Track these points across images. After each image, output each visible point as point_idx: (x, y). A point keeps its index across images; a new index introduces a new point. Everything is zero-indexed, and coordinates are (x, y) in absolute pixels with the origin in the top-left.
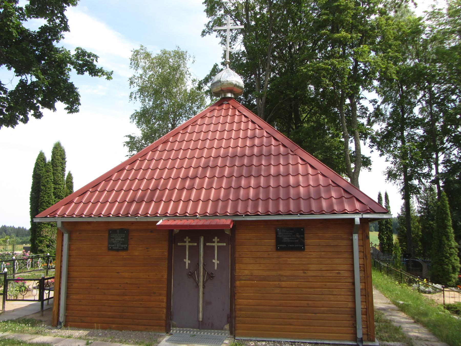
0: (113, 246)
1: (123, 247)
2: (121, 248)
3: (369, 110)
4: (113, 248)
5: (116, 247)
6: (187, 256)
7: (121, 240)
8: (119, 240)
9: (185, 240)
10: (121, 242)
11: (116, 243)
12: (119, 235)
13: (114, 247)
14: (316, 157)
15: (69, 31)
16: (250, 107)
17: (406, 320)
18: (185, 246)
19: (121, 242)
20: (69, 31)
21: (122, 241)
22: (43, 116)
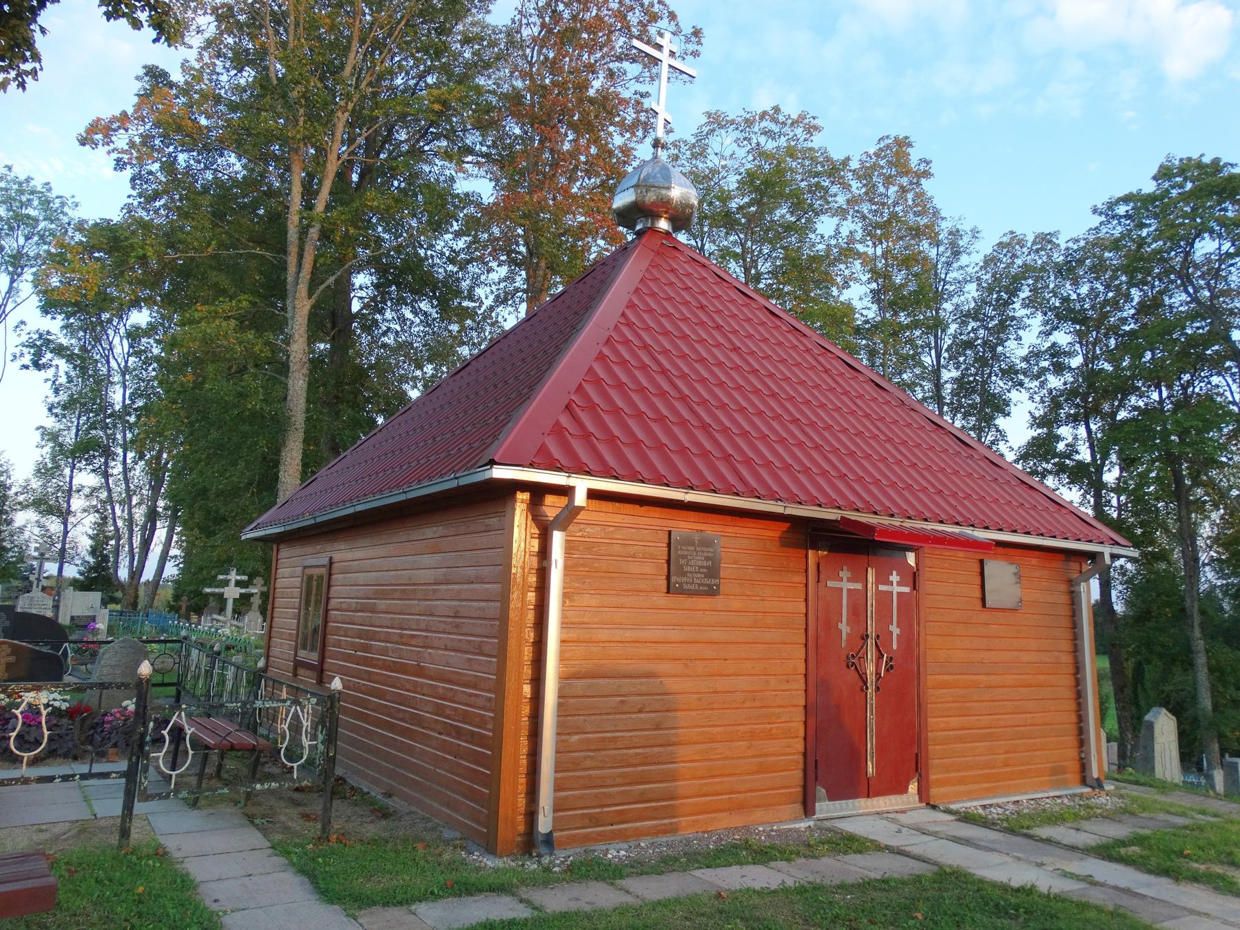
0: (685, 579)
1: (710, 586)
2: (706, 588)
3: (943, 214)
4: (685, 587)
5: (691, 584)
6: (844, 619)
7: (705, 563)
8: (699, 563)
9: (891, 578)
10: (705, 570)
11: (691, 572)
12: (698, 549)
13: (687, 583)
14: (284, 309)
15: (5, 92)
16: (300, 222)
17: (619, 635)
18: (849, 591)
19: (705, 570)
20: (5, 92)
21: (706, 567)
22: (906, 138)
